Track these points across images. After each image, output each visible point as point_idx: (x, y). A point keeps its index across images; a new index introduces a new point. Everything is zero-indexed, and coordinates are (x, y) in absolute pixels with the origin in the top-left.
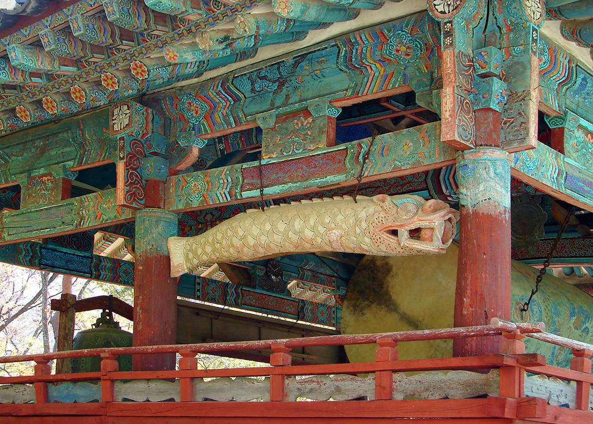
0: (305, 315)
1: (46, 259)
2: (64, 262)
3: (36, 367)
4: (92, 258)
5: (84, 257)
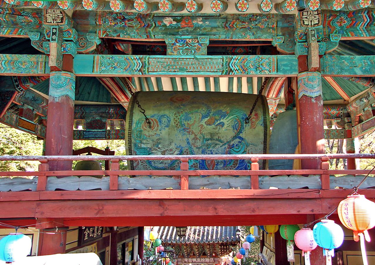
0: (367, 14)
1: (86, 136)
2: (93, 135)
3: (40, 166)
4: (106, 131)
5: (103, 131)
